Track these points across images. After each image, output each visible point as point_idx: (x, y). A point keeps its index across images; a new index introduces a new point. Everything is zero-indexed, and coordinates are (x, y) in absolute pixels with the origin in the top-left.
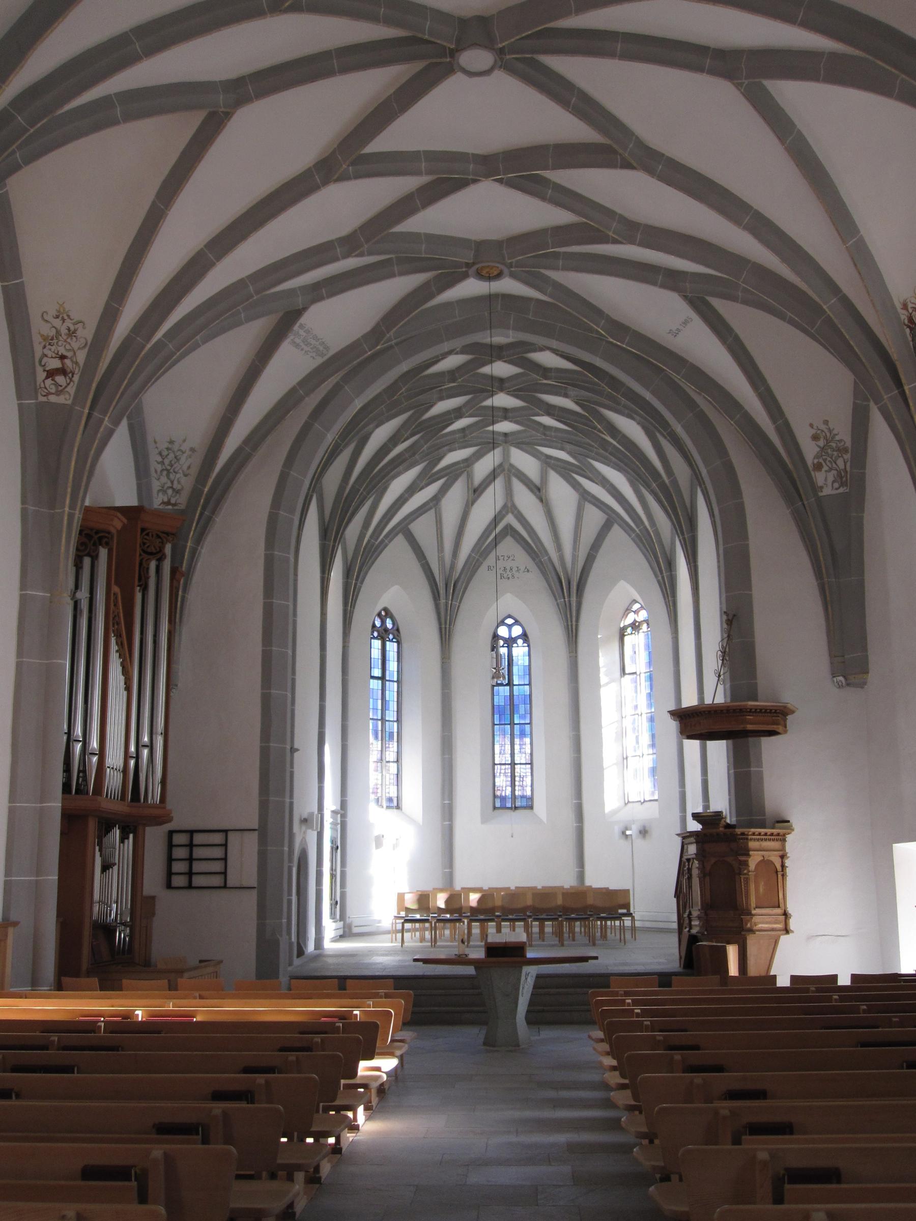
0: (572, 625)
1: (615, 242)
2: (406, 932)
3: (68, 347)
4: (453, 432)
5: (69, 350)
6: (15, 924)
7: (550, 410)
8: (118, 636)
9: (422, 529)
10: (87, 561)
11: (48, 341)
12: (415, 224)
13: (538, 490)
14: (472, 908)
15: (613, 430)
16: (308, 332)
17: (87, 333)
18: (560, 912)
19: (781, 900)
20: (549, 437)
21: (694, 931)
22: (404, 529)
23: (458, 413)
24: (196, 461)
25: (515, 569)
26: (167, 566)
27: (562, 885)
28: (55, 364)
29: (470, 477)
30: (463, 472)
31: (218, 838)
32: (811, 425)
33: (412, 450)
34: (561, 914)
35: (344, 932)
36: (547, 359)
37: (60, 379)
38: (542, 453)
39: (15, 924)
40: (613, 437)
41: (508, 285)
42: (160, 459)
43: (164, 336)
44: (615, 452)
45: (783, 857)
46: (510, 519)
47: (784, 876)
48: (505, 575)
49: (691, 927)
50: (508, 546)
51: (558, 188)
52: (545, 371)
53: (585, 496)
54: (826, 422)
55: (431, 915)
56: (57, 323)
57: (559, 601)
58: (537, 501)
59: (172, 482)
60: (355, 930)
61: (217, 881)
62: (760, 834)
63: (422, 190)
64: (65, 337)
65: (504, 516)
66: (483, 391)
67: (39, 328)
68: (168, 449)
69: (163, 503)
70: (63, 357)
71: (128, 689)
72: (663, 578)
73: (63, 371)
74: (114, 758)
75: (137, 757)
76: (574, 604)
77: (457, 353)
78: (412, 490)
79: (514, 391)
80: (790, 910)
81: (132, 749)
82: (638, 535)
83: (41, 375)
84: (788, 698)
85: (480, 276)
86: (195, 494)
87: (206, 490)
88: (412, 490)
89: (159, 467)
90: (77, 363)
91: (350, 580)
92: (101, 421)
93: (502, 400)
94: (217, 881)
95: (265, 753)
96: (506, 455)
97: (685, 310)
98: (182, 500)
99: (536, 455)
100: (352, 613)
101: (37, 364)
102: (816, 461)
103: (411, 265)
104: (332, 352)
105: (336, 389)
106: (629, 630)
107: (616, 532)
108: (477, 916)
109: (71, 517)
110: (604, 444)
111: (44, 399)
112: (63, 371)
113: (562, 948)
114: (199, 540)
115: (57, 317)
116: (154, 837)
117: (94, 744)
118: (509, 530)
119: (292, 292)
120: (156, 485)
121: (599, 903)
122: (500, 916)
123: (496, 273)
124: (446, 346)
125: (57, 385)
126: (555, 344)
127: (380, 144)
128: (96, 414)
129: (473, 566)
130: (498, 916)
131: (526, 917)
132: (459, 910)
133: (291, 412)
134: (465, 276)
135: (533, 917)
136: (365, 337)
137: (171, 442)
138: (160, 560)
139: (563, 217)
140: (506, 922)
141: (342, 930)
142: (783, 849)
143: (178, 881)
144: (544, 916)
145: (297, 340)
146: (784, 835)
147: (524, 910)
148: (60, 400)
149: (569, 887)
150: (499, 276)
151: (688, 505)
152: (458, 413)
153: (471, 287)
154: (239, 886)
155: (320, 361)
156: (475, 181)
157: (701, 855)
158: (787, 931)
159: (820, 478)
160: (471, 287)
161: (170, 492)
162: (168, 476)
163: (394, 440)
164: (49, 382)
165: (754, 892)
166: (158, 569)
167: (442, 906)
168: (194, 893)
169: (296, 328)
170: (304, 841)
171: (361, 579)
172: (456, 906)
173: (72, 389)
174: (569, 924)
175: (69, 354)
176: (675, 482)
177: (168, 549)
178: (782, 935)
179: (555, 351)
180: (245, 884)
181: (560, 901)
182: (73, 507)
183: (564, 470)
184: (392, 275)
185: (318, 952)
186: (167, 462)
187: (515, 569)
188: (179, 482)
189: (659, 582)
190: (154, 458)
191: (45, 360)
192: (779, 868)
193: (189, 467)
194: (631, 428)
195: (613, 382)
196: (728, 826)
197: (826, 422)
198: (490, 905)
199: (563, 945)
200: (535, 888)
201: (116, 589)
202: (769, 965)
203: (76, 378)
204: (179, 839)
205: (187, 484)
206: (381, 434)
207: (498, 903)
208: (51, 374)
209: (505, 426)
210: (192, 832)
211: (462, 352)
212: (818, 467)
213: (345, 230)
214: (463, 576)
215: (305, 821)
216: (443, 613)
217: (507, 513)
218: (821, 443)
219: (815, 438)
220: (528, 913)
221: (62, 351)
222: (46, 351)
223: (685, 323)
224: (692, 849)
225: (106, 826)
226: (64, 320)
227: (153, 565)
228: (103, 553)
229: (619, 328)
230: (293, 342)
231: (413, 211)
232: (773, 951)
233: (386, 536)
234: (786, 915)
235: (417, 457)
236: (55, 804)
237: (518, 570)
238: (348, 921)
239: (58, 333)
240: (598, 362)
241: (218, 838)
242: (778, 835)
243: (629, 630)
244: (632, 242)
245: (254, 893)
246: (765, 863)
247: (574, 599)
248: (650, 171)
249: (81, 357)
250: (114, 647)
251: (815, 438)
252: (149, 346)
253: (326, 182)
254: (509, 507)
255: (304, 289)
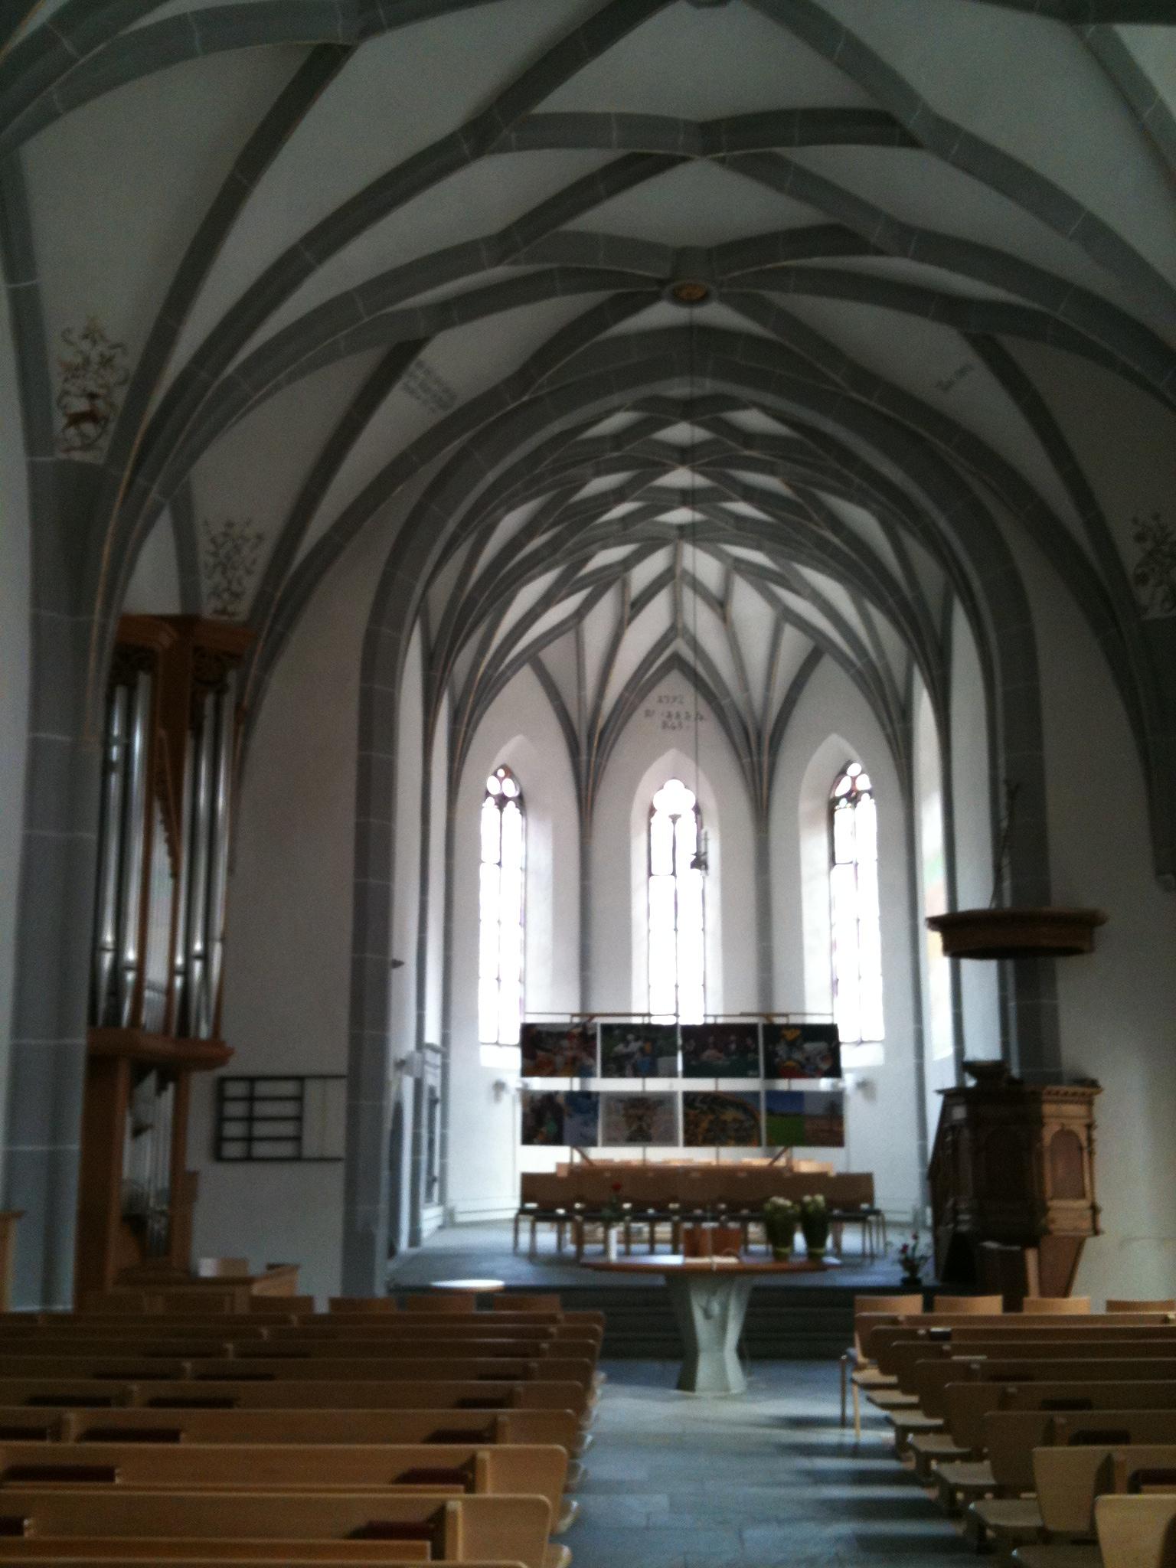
0: (762, 794)
1: (879, 252)
3: (100, 381)
4: (610, 523)
5: (102, 386)
6: (19, 1215)
7: (749, 494)
8: (164, 799)
9: (555, 656)
10: (120, 694)
11: (73, 371)
12: (596, 220)
13: (720, 605)
15: (836, 524)
16: (428, 372)
17: (129, 362)
19: (1088, 1188)
20: (745, 531)
21: (964, 1228)
22: (532, 657)
23: (618, 495)
24: (263, 554)
25: (683, 716)
26: (229, 701)
28: (81, 405)
29: (625, 586)
30: (618, 578)
31: (289, 1088)
32: (1135, 521)
33: (553, 546)
35: (445, 1222)
36: (752, 419)
37: (88, 428)
38: (728, 555)
39: (19, 1215)
40: (836, 532)
41: (717, 314)
42: (212, 548)
43: (237, 370)
44: (835, 553)
45: (1090, 1127)
46: (680, 646)
47: (1091, 1153)
48: (670, 724)
49: (957, 1223)
50: (675, 684)
51: (802, 173)
52: (748, 438)
53: (786, 616)
54: (1156, 517)
56: (86, 345)
57: (744, 761)
58: (718, 623)
59: (230, 582)
61: (286, 1149)
62: (1057, 1093)
63: (608, 171)
64: (96, 367)
65: (671, 641)
66: (655, 464)
67: (60, 352)
68: (226, 535)
69: (216, 612)
70: (92, 396)
71: (175, 874)
72: (894, 731)
73: (91, 416)
74: (156, 972)
75: (186, 972)
76: (765, 766)
77: (628, 410)
78: (547, 601)
79: (707, 464)
80: (1101, 1201)
81: (179, 960)
82: (859, 672)
83: (60, 421)
84: (1089, 901)
85: (678, 299)
86: (262, 598)
87: (279, 594)
88: (547, 601)
89: (211, 560)
90: (112, 405)
91: (458, 727)
92: (146, 492)
93: (680, 477)
94: (286, 1149)
95: (358, 968)
96: (676, 557)
97: (966, 355)
98: (242, 609)
99: (720, 555)
100: (460, 771)
101: (54, 404)
102: (1139, 571)
103: (577, 279)
104: (457, 404)
105: (462, 455)
106: (843, 802)
107: (828, 666)
109: (104, 628)
110: (822, 544)
111: (62, 456)
112: (91, 416)
114: (268, 665)
115: (86, 337)
116: (201, 1084)
117: (131, 955)
118: (677, 662)
119: (410, 313)
120: (206, 585)
123: (700, 294)
124: (615, 399)
125: (83, 435)
126: (769, 399)
127: (560, 100)
128: (141, 481)
129: (626, 707)
133: (399, 489)
134: (653, 298)
136: (508, 382)
137: (230, 525)
138: (220, 692)
139: (796, 214)
142: (1090, 1115)
143: (232, 1150)
145: (413, 384)
146: (1091, 1095)
148: (87, 457)
150: (704, 299)
151: (939, 631)
152: (618, 495)
153: (662, 314)
154: (316, 1155)
155: (441, 415)
156: (684, 159)
157: (974, 1121)
158: (1096, 1232)
159: (1143, 594)
160: (662, 314)
161: (226, 596)
162: (224, 573)
163: (529, 530)
164: (72, 431)
165: (1053, 1172)
166: (218, 707)
168: (254, 1169)
169: (412, 367)
170: (399, 1093)
171: (473, 724)
173: (105, 443)
175: (102, 391)
176: (920, 599)
177: (232, 677)
178: (1089, 1236)
179: (765, 409)
180: (328, 1153)
182: (106, 614)
183: (758, 576)
184: (549, 294)
185: (415, 1250)
186: (222, 552)
187: (683, 716)
188: (240, 583)
189: (887, 737)
190: (204, 545)
191: (66, 400)
192: (1085, 1144)
193: (254, 562)
194: (863, 520)
195: (847, 457)
196: (1012, 1081)
197: (1156, 517)
201: (162, 733)
203: (112, 426)
204: (235, 1089)
205: (251, 585)
206: (511, 522)
208: (76, 419)
209: (681, 515)
210: (252, 1080)
211: (635, 407)
212: (1142, 579)
213: (495, 224)
214: (612, 724)
215: (401, 1064)
216: (583, 779)
217: (676, 636)
218: (1149, 545)
219: (1140, 538)
221: (92, 387)
222: (68, 386)
223: (962, 372)
224: (959, 1113)
225: (139, 1074)
226: (94, 342)
227: (209, 701)
228: (144, 680)
229: (867, 379)
230: (408, 389)
231: (595, 201)
233: (509, 666)
234: (1095, 1210)
235: (558, 556)
236: (79, 1041)
237: (688, 717)
238: (450, 1204)
239: (87, 361)
240: (829, 426)
241: (289, 1088)
242: (1083, 1094)
243: (843, 802)
244: (904, 253)
245: (340, 1169)
246: (1066, 1134)
247: (765, 759)
248: (943, 153)
249: (120, 396)
250: (158, 816)
251: (1140, 538)
252: (217, 383)
253: (478, 153)
254: (675, 630)
255: (426, 309)
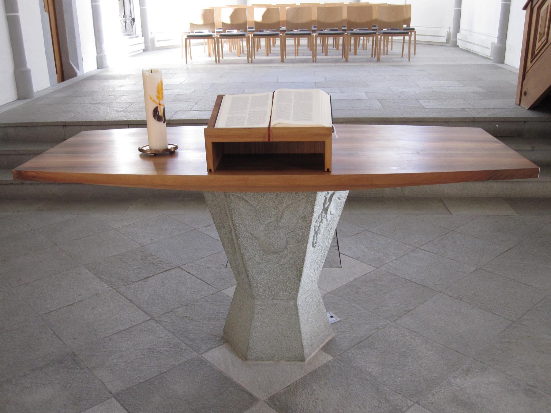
2: (193, 46)
14: (256, 23)
18: (315, 27)
27: (368, 2)
34: (316, 29)
55: (216, 30)
60: (158, 44)
108: (263, 31)
113: (378, 64)
121: (385, 18)
122: (285, 31)
130: (283, 31)
131: (311, 32)
132: (243, 26)
135: (318, 32)
140: (187, 42)
141: (144, 45)
144: (326, 31)
147: (307, 25)
149: (323, 4)
167: (228, 21)
172: (242, 21)
174: (384, 39)
181: (345, 16)
198: (274, 20)
199: (347, 61)
200: (319, 4)
202: (360, 122)
207: (283, 17)
220: (313, 29)
232: (197, 124)
238: (150, 36)
